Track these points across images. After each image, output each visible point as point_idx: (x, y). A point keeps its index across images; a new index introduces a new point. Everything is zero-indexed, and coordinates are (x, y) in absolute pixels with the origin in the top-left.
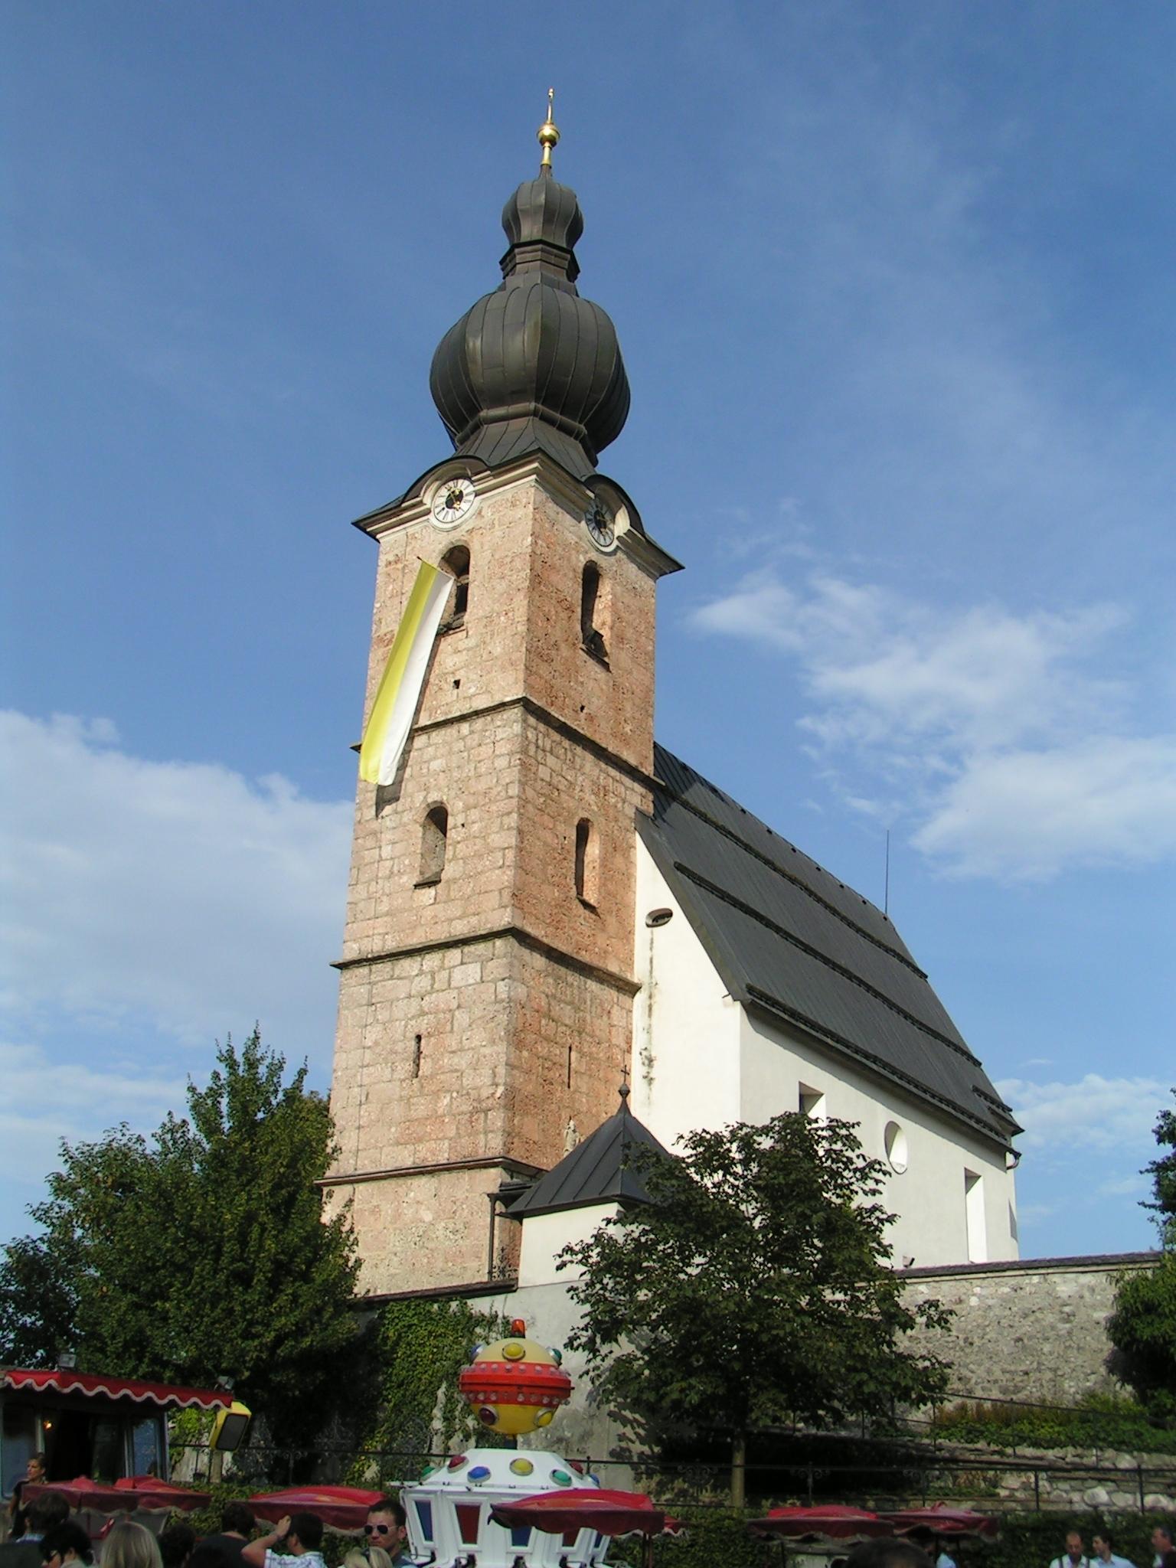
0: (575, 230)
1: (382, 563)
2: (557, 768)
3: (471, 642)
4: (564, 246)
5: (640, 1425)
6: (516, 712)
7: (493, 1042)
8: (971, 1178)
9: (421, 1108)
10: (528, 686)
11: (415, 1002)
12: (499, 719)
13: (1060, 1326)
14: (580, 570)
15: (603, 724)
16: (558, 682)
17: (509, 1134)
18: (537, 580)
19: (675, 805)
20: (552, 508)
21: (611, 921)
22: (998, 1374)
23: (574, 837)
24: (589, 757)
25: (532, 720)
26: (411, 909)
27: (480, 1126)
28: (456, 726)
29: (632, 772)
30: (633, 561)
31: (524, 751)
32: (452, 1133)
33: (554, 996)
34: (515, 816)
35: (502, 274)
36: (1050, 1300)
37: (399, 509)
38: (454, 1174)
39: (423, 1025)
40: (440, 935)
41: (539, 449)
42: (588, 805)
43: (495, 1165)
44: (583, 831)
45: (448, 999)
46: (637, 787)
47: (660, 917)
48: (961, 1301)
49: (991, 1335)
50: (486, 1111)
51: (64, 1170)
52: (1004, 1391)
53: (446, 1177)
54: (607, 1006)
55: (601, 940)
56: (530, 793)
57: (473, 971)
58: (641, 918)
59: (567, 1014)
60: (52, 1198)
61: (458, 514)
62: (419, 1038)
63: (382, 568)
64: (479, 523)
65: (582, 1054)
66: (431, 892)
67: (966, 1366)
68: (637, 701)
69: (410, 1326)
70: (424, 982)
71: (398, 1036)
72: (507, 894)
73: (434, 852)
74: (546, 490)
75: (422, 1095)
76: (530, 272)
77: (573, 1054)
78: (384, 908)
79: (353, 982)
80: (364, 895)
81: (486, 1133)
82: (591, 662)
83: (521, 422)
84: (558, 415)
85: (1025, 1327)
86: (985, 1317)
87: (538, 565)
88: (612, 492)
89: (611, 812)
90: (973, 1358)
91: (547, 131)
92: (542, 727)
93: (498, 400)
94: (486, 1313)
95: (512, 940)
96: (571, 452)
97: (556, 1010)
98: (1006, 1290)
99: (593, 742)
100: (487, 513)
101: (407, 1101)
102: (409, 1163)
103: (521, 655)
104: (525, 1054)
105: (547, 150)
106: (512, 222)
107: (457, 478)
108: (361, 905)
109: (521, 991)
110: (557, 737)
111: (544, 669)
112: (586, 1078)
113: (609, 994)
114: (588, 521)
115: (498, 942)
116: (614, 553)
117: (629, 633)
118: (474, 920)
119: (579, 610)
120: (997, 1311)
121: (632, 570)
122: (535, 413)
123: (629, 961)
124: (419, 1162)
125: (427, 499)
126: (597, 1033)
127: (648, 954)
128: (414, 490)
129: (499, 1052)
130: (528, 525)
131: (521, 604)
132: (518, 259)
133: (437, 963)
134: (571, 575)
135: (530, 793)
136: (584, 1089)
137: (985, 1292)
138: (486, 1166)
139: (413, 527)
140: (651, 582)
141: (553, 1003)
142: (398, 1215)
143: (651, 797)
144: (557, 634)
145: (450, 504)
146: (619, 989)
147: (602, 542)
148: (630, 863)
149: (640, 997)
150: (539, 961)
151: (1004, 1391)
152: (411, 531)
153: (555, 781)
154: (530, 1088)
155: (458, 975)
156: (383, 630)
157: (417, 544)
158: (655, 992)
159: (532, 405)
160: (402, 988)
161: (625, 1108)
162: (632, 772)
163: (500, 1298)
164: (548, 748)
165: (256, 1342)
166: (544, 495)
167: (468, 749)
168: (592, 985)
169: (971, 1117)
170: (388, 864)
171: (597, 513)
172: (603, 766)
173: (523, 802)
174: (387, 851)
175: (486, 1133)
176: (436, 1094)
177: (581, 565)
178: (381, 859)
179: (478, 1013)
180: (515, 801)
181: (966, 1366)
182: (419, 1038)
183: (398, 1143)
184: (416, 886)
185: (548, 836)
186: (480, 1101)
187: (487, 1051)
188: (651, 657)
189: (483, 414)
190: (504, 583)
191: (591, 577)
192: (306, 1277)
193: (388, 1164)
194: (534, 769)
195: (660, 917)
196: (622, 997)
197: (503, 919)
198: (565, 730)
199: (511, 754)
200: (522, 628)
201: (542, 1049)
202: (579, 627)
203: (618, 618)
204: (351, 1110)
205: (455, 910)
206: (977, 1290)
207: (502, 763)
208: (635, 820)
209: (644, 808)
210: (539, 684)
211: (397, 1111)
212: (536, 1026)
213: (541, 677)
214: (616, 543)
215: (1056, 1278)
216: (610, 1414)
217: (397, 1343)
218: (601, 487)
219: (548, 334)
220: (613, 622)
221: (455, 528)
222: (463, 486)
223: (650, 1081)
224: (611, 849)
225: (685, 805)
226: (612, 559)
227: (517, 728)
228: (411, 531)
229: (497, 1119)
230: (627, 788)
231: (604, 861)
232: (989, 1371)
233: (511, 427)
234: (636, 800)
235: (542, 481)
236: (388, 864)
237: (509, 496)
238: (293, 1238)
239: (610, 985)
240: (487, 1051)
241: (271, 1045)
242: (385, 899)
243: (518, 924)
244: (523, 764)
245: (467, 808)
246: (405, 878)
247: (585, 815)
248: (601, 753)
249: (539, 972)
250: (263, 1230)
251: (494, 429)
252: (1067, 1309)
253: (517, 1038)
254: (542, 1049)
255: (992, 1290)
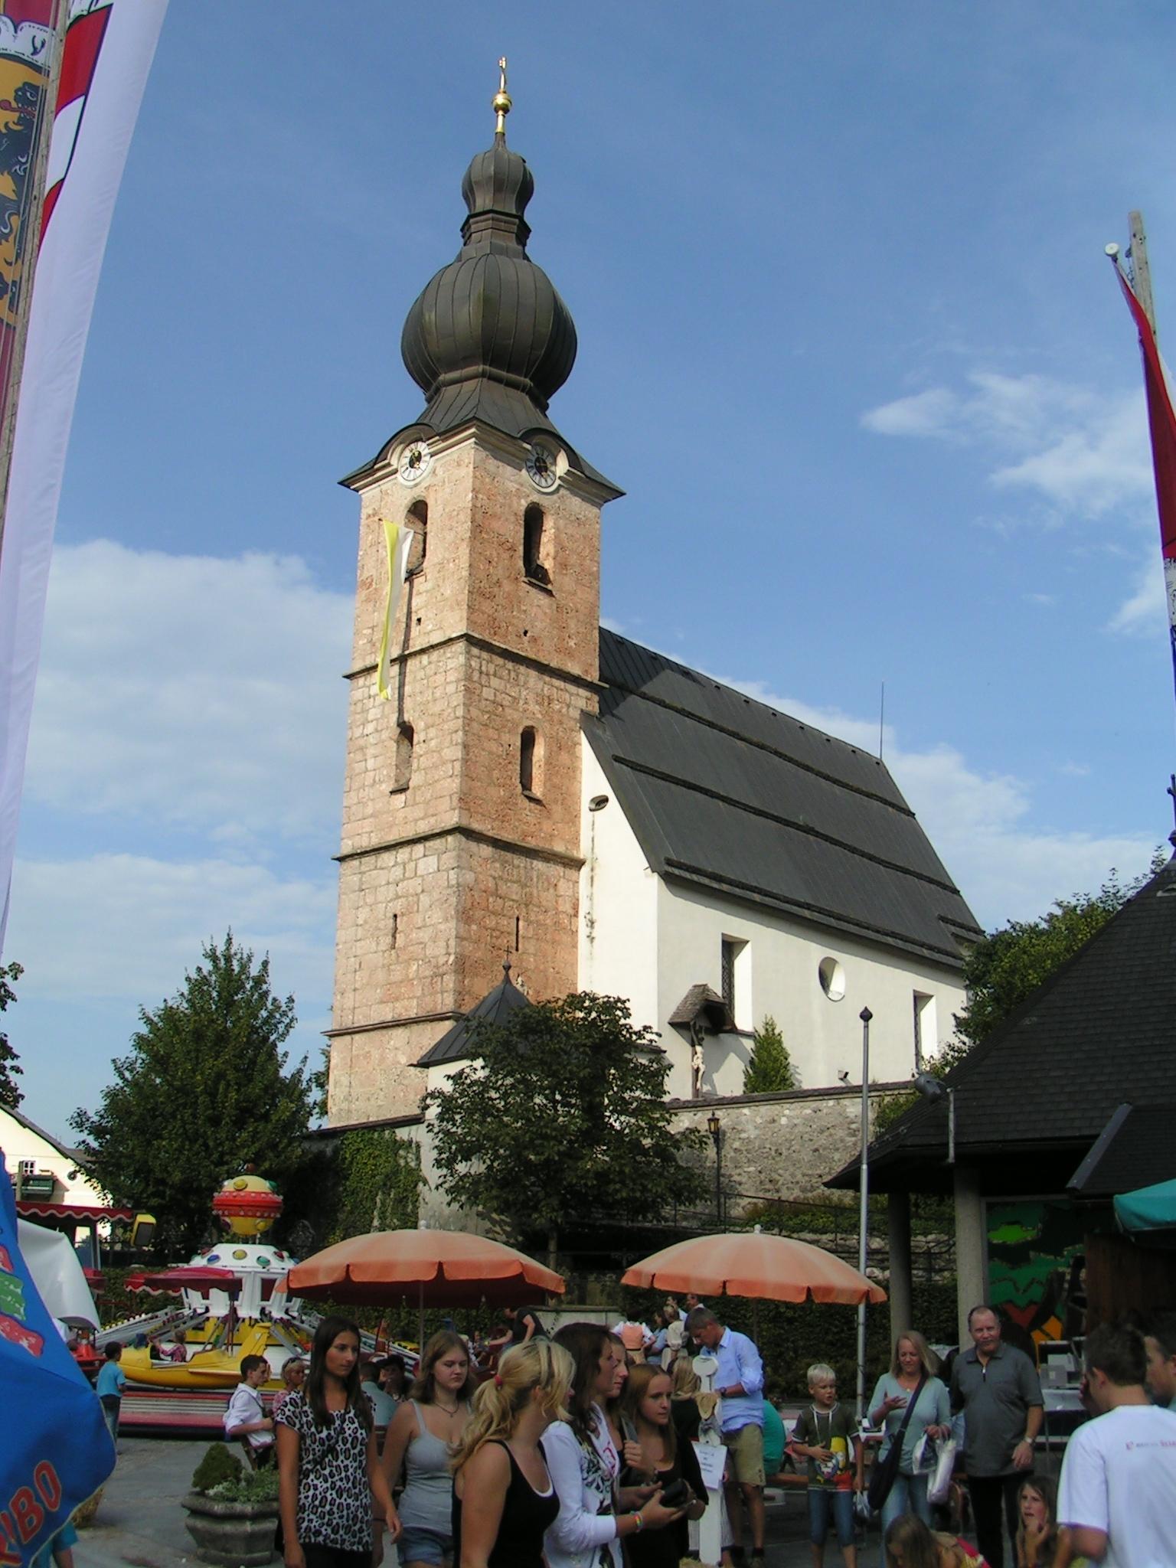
0: (525, 191)
1: (363, 516)
2: (502, 688)
3: (429, 585)
4: (514, 212)
5: (506, 1224)
6: (461, 646)
7: (447, 920)
8: (920, 1000)
9: (397, 976)
10: (471, 622)
11: (392, 887)
12: (449, 651)
13: (848, 1139)
14: (522, 513)
15: (547, 643)
16: (501, 615)
17: (460, 993)
18: (478, 529)
19: (633, 699)
20: (492, 464)
21: (557, 810)
22: (799, 1177)
23: (519, 744)
24: (533, 673)
25: (475, 651)
26: (388, 812)
27: (438, 987)
28: (418, 658)
29: (577, 681)
30: (576, 494)
31: (468, 678)
32: (419, 994)
33: (501, 878)
34: (460, 733)
35: (462, 241)
36: (841, 1119)
37: (372, 470)
38: (421, 1026)
39: (398, 907)
40: (409, 833)
41: (474, 418)
42: (532, 713)
43: (448, 1018)
44: (528, 739)
45: (414, 885)
46: (582, 692)
47: (600, 802)
48: (774, 1121)
49: (796, 1147)
50: (442, 975)
51: (144, 1030)
52: (804, 1190)
53: (415, 1027)
54: (553, 881)
55: (547, 826)
56: (475, 712)
57: (432, 862)
58: (585, 803)
59: (514, 891)
60: (135, 1053)
61: (419, 472)
62: (395, 916)
63: (363, 522)
64: (434, 481)
65: (529, 923)
66: (402, 797)
67: (776, 1171)
68: (582, 618)
69: (358, 1150)
70: (397, 872)
71: (381, 916)
72: (455, 798)
73: (404, 763)
74: (485, 449)
75: (398, 962)
76: (484, 237)
77: (521, 923)
78: (369, 811)
79: (348, 872)
80: (356, 801)
81: (442, 993)
82: (533, 591)
83: (471, 384)
84: (504, 373)
85: (822, 1140)
86: (791, 1133)
87: (479, 516)
88: (550, 439)
89: (556, 717)
90: (781, 1165)
91: (500, 99)
92: (485, 655)
93: (452, 366)
94: (406, 1138)
95: (458, 836)
96: (517, 408)
97: (503, 889)
98: (808, 1111)
99: (535, 661)
100: (440, 472)
101: (387, 967)
102: (389, 1018)
103: (464, 597)
104: (474, 927)
105: (500, 118)
106: (469, 194)
107: (417, 441)
108: (354, 808)
109: (470, 877)
110: (500, 661)
111: (487, 606)
112: (533, 942)
113: (555, 870)
114: (529, 469)
115: (450, 838)
116: (557, 490)
117: (573, 559)
118: (432, 820)
119: (521, 548)
120: (800, 1128)
121: (575, 503)
122: (483, 375)
123: (575, 841)
124: (397, 1017)
125: (394, 461)
126: (544, 903)
127: (591, 834)
128: (382, 454)
129: (450, 928)
130: (469, 483)
131: (464, 551)
132: (473, 228)
133: (407, 856)
134: (513, 518)
135: (475, 712)
136: (532, 950)
137: (792, 1114)
138: (442, 1019)
139: (386, 484)
140: (595, 510)
141: (500, 883)
142: (383, 1059)
143: (596, 698)
144: (499, 572)
145: (412, 464)
146: (565, 865)
147: (544, 483)
148: (575, 758)
149: (585, 870)
150: (486, 850)
151: (804, 1190)
152: (384, 487)
153: (498, 699)
154: (479, 954)
155: (421, 864)
156: (366, 574)
157: (389, 499)
158: (596, 865)
159: (480, 368)
160: (382, 877)
161: (507, 980)
162: (577, 681)
163: (414, 1127)
164: (492, 672)
165: (226, 1168)
166: (484, 454)
167: (427, 677)
168: (538, 865)
169: (922, 945)
170: (372, 774)
171: (538, 460)
172: (547, 679)
173: (468, 721)
174: (371, 763)
175: (442, 993)
176: (408, 962)
177: (523, 509)
178: (367, 770)
179: (436, 895)
180: (460, 721)
181: (776, 1171)
182: (395, 916)
183: (382, 1002)
184: (392, 793)
185: (493, 746)
186: (437, 967)
187: (442, 927)
188: (596, 576)
189: (441, 378)
190: (453, 534)
191: (533, 519)
192: (266, 1117)
193: (375, 1018)
194: (478, 692)
195: (600, 802)
196: (568, 871)
197: (452, 819)
198: (507, 655)
199: (458, 681)
200: (465, 573)
201: (491, 922)
202: (521, 563)
203: (560, 547)
204: (349, 976)
205: (418, 812)
206: (787, 1112)
207: (451, 688)
208: (581, 721)
209: (590, 708)
210: (480, 619)
211: (381, 975)
212: (484, 904)
213: (483, 613)
214: (558, 482)
215: (846, 1102)
216: (479, 1214)
217: (351, 1163)
218: (537, 439)
219: (489, 304)
220: (557, 552)
221: (416, 485)
222: (422, 447)
223: (592, 939)
224: (555, 749)
225: (644, 696)
226: (555, 497)
227: (462, 659)
228: (384, 487)
229: (450, 981)
230: (571, 695)
231: (549, 761)
232: (793, 1175)
233: (467, 390)
234: (581, 703)
235: (481, 442)
236: (372, 774)
237: (455, 456)
238: (255, 1089)
239: (556, 863)
240: (442, 927)
241: (243, 944)
242: (370, 803)
243: (464, 823)
244: (467, 689)
245: (427, 727)
246: (384, 786)
247: (529, 723)
248: (543, 668)
249: (486, 860)
250: (228, 1085)
251: (452, 390)
252: (853, 1126)
253: (465, 915)
254: (491, 922)
255: (798, 1112)
